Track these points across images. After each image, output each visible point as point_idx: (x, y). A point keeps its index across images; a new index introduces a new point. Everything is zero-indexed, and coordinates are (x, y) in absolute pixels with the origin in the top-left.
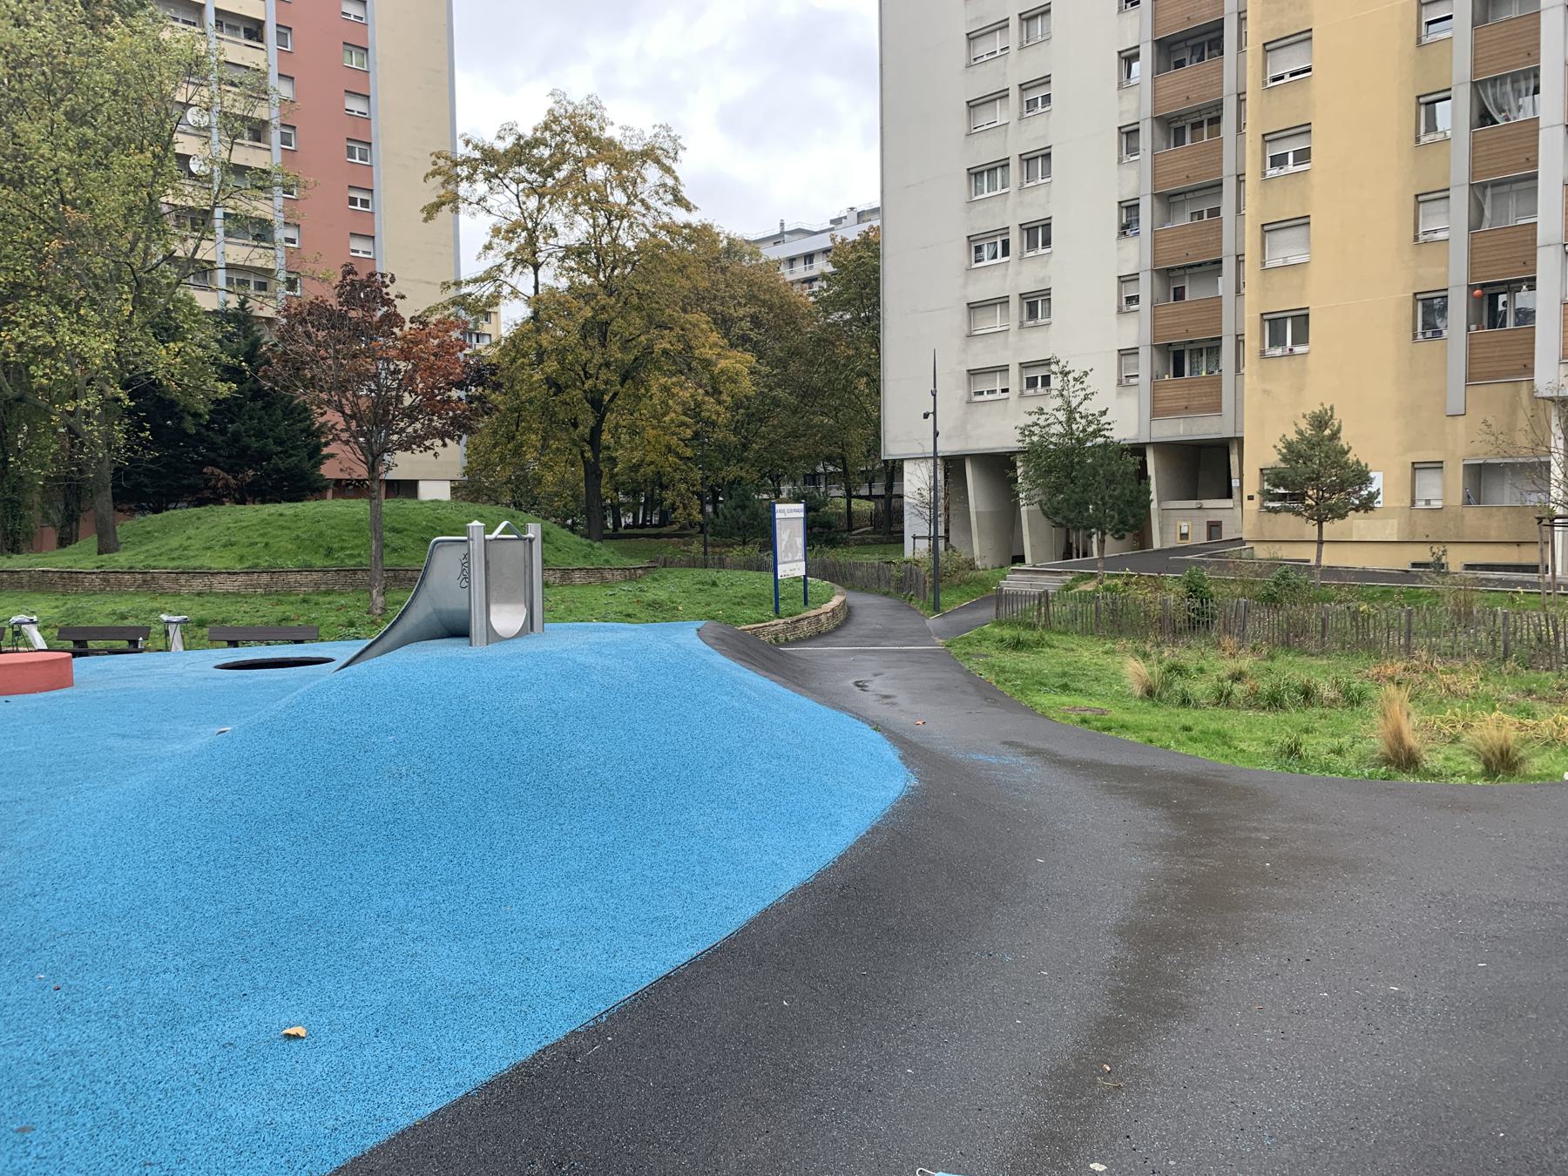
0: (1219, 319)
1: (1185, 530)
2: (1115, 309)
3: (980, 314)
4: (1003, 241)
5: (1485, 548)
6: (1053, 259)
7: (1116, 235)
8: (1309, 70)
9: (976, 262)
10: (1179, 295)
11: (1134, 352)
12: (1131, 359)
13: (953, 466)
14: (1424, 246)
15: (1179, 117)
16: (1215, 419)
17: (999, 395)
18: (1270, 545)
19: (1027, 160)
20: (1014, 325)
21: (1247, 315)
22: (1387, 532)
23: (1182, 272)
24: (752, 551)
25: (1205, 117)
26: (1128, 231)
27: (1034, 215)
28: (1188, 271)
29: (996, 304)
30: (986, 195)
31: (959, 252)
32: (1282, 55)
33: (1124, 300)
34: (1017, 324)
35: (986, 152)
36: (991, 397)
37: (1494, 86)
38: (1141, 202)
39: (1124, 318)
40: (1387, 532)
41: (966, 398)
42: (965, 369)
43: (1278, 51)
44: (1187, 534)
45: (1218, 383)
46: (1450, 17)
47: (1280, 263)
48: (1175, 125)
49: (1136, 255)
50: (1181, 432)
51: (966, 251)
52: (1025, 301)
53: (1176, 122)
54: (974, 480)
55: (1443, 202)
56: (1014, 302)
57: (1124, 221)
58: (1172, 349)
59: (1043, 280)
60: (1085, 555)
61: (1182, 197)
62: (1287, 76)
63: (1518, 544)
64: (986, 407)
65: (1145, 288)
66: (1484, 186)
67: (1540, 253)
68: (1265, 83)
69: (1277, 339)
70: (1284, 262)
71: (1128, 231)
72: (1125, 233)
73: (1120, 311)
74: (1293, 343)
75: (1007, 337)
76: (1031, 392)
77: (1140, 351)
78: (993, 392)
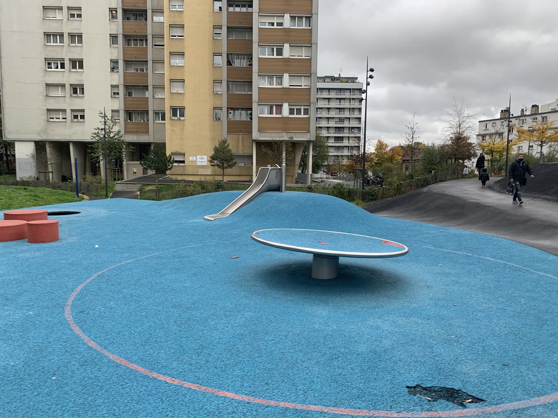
0: (147, 104)
1: (135, 171)
2: (110, 96)
3: (51, 89)
4: (61, 63)
5: (193, 176)
6: (84, 74)
7: (110, 71)
8: (183, 36)
9: (48, 68)
10: (130, 94)
11: (118, 111)
12: (116, 114)
13: (40, 146)
14: (216, 95)
15: (130, 36)
16: (147, 136)
17: (61, 120)
18: (205, 176)
19: (72, 36)
20: (68, 95)
21: (166, 106)
22: (208, 172)
23: (132, 87)
24: (14, 175)
25: (138, 39)
26: (114, 70)
27: (76, 56)
28: (134, 87)
29: (59, 86)
30: (52, 44)
31: (42, 64)
32: (174, 29)
33: (113, 93)
34: (69, 95)
35: (54, 28)
36: (57, 120)
37: (236, 55)
38: (119, 61)
39: (114, 99)
40: (208, 172)
41: (46, 119)
42: (45, 108)
43: (174, 28)
44: (136, 172)
45: (148, 124)
46: (221, 34)
47: (176, 92)
48: (128, 38)
49: (117, 78)
50: (135, 139)
51: (44, 64)
52: (72, 87)
53: (129, 37)
54: (74, 151)
55: (220, 84)
56: (68, 87)
57: (112, 66)
58: (128, 111)
59: (80, 81)
60: (122, 179)
61: (131, 62)
62: (177, 36)
63: (240, 175)
64: (54, 124)
65: (121, 90)
66: (230, 81)
67: (253, 103)
68: (170, 37)
69: (175, 114)
70: (177, 92)
71: (114, 70)
72: (113, 71)
73: (111, 97)
74: (180, 116)
75: (65, 99)
76: (76, 120)
77: (120, 111)
78: (59, 118)
